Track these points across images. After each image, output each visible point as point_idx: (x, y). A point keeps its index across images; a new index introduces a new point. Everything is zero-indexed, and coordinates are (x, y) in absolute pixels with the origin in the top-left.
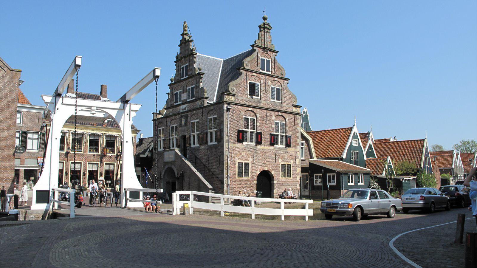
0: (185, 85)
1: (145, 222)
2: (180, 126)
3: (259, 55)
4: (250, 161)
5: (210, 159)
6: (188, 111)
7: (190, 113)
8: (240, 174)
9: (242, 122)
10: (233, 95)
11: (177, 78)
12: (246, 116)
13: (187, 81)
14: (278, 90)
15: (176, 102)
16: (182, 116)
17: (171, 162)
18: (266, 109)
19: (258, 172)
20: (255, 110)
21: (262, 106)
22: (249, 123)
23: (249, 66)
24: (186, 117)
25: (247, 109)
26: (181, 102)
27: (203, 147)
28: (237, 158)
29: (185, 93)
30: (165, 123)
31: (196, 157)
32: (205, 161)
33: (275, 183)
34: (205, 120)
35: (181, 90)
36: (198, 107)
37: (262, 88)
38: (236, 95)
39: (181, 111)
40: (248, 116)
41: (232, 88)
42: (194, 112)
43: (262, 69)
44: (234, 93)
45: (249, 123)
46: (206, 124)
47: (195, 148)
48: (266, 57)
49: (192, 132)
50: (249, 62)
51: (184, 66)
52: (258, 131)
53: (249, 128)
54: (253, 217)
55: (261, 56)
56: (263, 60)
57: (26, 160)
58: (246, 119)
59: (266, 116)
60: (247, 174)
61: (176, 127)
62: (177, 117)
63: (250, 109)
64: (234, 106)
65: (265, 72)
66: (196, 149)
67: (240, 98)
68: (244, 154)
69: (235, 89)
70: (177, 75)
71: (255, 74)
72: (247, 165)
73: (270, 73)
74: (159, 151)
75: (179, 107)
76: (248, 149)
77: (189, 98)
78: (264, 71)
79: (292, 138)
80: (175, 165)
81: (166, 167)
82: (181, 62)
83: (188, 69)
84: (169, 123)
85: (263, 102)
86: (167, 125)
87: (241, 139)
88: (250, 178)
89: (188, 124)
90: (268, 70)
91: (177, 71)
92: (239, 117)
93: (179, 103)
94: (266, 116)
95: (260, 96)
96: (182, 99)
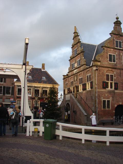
0: (76, 59)
1: (65, 126)
2: (74, 81)
3: (114, 39)
4: (110, 99)
5: (88, 98)
6: (77, 73)
7: (78, 74)
8: (104, 107)
9: (105, 77)
10: (99, 61)
11: (73, 56)
12: (108, 73)
13: (77, 57)
14: (120, 42)
15: (73, 69)
16: (75, 76)
17: (69, 101)
18: (120, 69)
19: (116, 106)
20: (113, 70)
21: (117, 67)
22: (110, 77)
23: (109, 45)
24: (77, 76)
25: (108, 69)
26: (74, 69)
27: (84, 92)
28: (102, 98)
29: (76, 63)
30: (68, 80)
31: (81, 98)
32: (85, 99)
33: (121, 104)
34: (85, 76)
35: (74, 62)
36: (82, 70)
37: (117, 57)
38: (101, 62)
39: (75, 73)
40: (109, 73)
41: (99, 58)
42: (80, 73)
43: (116, 47)
44: (100, 60)
45: (110, 77)
46: (85, 79)
47: (80, 93)
48: (119, 40)
49: (80, 84)
50: (108, 43)
51: (75, 49)
52: (116, 82)
53: (110, 80)
54: (108, 144)
55: (116, 39)
56: (117, 42)
57: (5, 99)
58: (108, 76)
59: (120, 73)
60: (108, 107)
61: (73, 81)
62: (73, 76)
63: (110, 69)
64: (100, 67)
65: (119, 48)
66: (81, 93)
67: (103, 63)
68: (106, 95)
69: (100, 58)
70: (73, 55)
71: (112, 49)
72: (108, 101)
73: (122, 49)
74: (88, 91)
75: (74, 71)
76: (110, 92)
77: (78, 66)
78: (118, 47)
79: (119, 85)
80: (70, 102)
81: (66, 103)
82: (74, 47)
83: (77, 50)
84: (69, 80)
85: (118, 65)
86: (69, 81)
87: (105, 86)
88: (111, 109)
89: (78, 79)
90: (120, 47)
91: (73, 52)
92: (103, 73)
93: (74, 69)
94: (120, 73)
95: (116, 62)
96: (75, 67)
